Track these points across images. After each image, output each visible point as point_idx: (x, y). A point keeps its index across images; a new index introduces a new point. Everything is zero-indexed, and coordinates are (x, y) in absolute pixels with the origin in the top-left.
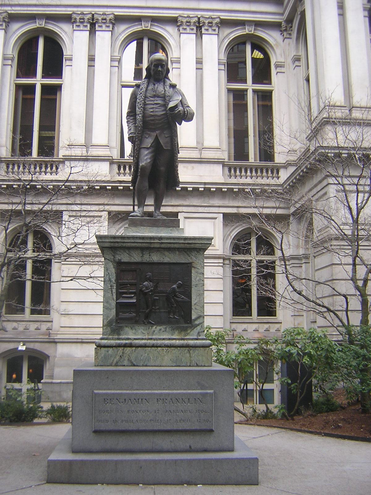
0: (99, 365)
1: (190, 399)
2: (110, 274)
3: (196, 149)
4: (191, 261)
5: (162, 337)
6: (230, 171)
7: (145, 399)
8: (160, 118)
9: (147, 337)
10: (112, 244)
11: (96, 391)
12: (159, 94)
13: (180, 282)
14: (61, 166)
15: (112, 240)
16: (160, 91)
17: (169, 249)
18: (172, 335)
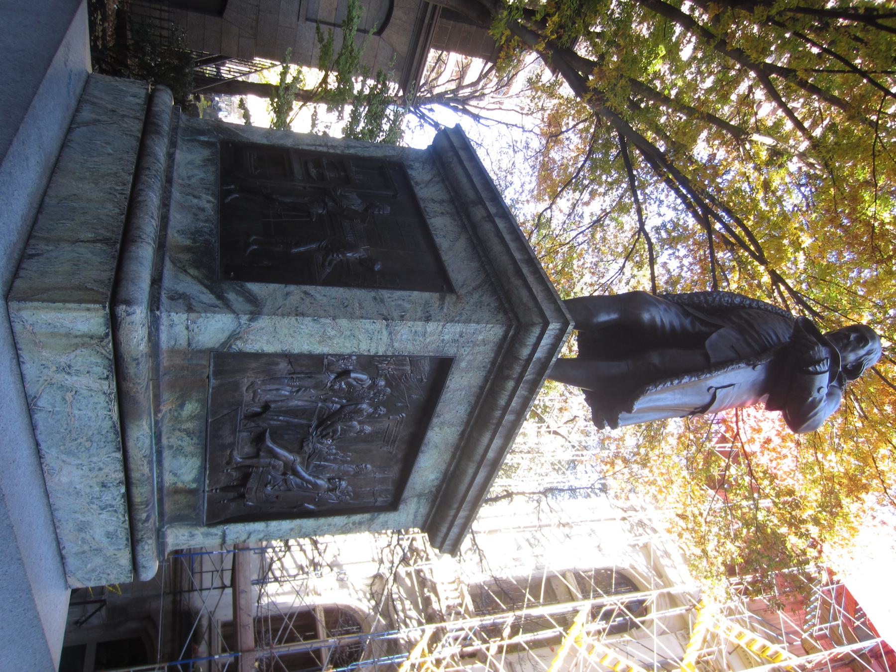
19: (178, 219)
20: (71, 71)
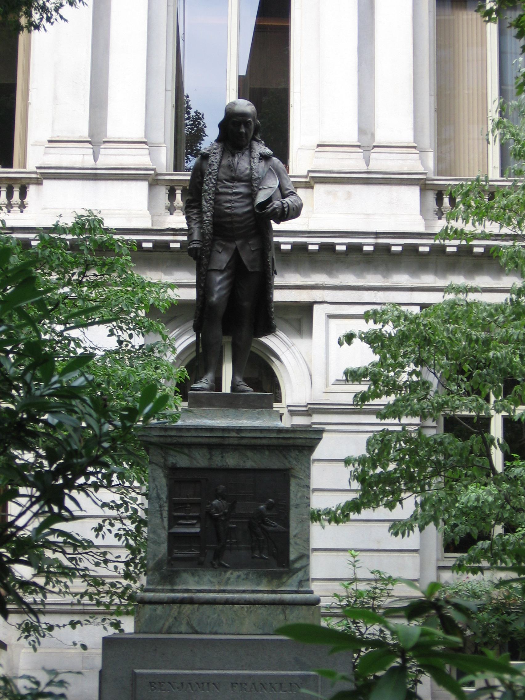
0: (142, 631)
1: (283, 685)
2: (159, 487)
3: (357, 149)
4: (288, 465)
5: (241, 588)
6: (439, 200)
7: (214, 684)
8: (242, 218)
9: (217, 588)
10: (162, 440)
11: (137, 671)
12: (242, 176)
13: (271, 500)
14: (32, 190)
15: (162, 433)
16: (243, 169)
18: (258, 585)
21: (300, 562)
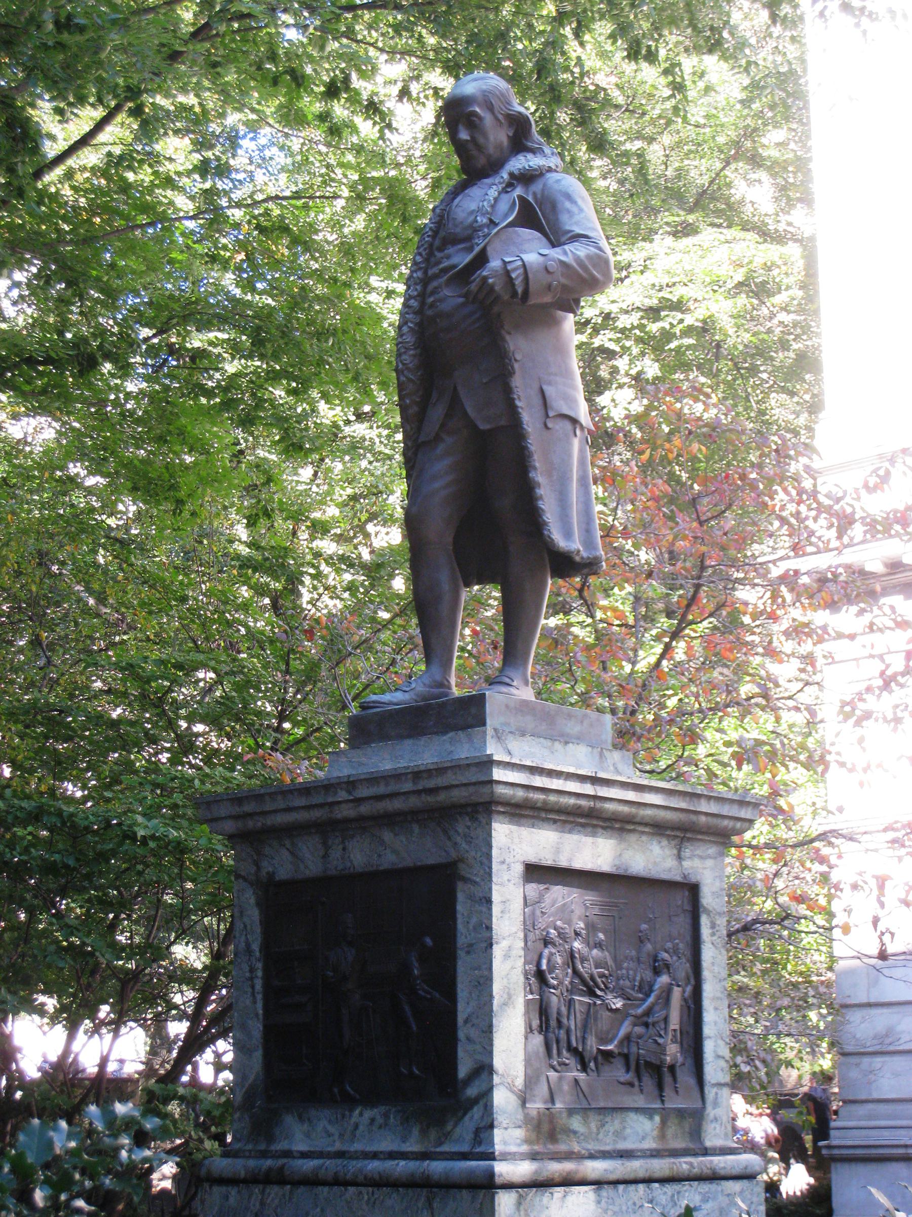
17: (391, 820)
19: (386, 1144)
20: (641, 1091)
21: (477, 1083)
